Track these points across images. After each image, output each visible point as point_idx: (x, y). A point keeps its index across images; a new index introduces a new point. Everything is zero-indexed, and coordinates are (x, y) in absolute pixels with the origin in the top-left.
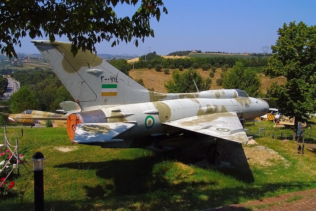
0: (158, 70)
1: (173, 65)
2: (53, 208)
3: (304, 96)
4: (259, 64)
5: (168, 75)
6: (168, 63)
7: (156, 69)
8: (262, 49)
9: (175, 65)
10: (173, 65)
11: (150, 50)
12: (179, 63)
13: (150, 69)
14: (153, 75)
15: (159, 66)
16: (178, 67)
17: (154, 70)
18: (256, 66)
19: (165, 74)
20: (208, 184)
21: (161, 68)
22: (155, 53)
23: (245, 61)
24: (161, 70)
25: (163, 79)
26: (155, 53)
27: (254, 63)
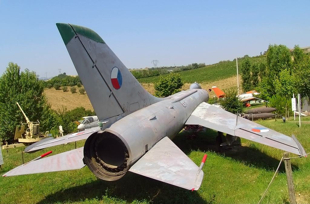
0: (58, 88)
1: (73, 83)
2: (296, 97)
3: (291, 114)
4: (150, 75)
5: (66, 92)
6: (67, 82)
7: (55, 88)
8: (152, 62)
9: (74, 82)
10: (73, 83)
11: (60, 72)
12: (77, 80)
13: (50, 88)
14: (52, 94)
15: (58, 85)
16: (76, 84)
17: (53, 89)
18: (147, 77)
19: (64, 91)
20: (173, 166)
21: (60, 86)
22: (65, 73)
23: (137, 73)
24: (60, 88)
25: (61, 96)
26: (65, 73)
27: (145, 75)
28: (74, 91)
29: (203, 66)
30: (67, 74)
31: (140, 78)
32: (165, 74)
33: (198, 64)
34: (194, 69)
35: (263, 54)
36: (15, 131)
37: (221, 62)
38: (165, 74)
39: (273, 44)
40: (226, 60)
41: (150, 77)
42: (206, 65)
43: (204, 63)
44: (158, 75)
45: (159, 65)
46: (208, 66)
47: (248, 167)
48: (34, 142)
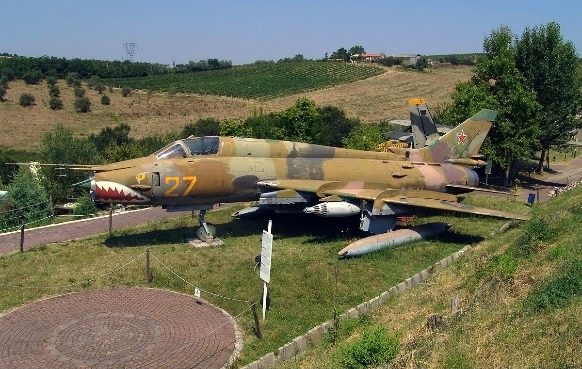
18: (123, 76)
28: (311, 91)
29: (228, 66)
30: (306, 57)
31: (109, 77)
32: (158, 74)
33: (219, 61)
34: (212, 69)
35: (329, 56)
36: (327, 146)
37: (258, 63)
38: (158, 74)
39: (566, 36)
40: (267, 60)
41: (131, 77)
42: (233, 65)
43: (230, 61)
44: (145, 75)
45: (138, 58)
46: (237, 66)
47: (449, 245)
48: (411, 168)
